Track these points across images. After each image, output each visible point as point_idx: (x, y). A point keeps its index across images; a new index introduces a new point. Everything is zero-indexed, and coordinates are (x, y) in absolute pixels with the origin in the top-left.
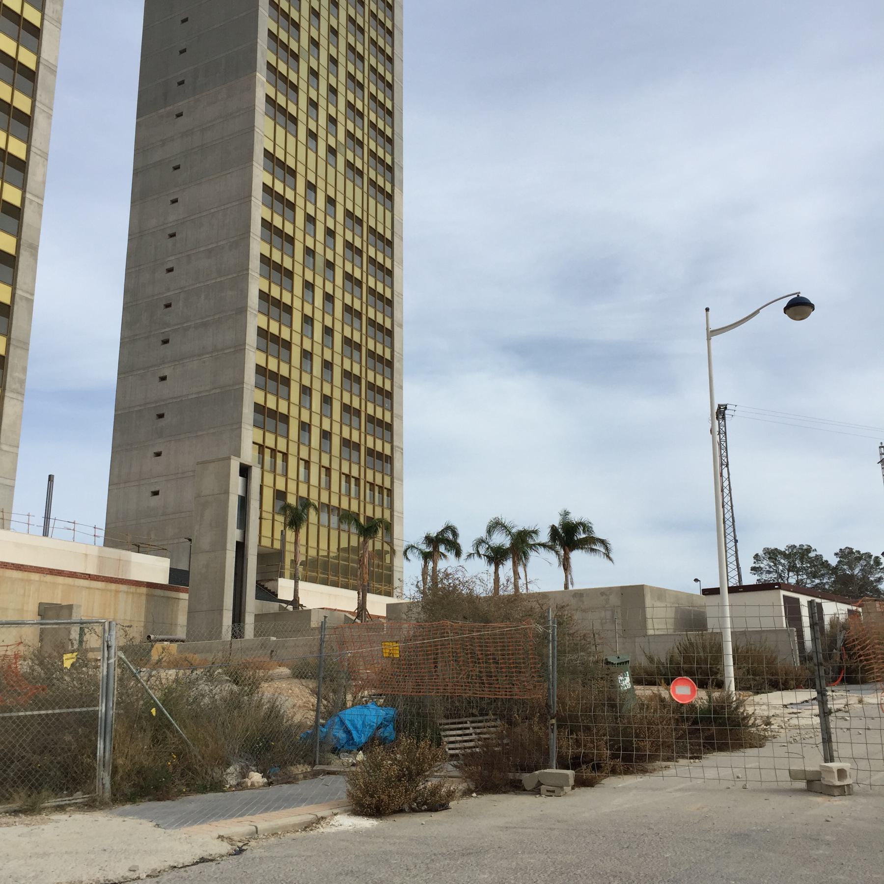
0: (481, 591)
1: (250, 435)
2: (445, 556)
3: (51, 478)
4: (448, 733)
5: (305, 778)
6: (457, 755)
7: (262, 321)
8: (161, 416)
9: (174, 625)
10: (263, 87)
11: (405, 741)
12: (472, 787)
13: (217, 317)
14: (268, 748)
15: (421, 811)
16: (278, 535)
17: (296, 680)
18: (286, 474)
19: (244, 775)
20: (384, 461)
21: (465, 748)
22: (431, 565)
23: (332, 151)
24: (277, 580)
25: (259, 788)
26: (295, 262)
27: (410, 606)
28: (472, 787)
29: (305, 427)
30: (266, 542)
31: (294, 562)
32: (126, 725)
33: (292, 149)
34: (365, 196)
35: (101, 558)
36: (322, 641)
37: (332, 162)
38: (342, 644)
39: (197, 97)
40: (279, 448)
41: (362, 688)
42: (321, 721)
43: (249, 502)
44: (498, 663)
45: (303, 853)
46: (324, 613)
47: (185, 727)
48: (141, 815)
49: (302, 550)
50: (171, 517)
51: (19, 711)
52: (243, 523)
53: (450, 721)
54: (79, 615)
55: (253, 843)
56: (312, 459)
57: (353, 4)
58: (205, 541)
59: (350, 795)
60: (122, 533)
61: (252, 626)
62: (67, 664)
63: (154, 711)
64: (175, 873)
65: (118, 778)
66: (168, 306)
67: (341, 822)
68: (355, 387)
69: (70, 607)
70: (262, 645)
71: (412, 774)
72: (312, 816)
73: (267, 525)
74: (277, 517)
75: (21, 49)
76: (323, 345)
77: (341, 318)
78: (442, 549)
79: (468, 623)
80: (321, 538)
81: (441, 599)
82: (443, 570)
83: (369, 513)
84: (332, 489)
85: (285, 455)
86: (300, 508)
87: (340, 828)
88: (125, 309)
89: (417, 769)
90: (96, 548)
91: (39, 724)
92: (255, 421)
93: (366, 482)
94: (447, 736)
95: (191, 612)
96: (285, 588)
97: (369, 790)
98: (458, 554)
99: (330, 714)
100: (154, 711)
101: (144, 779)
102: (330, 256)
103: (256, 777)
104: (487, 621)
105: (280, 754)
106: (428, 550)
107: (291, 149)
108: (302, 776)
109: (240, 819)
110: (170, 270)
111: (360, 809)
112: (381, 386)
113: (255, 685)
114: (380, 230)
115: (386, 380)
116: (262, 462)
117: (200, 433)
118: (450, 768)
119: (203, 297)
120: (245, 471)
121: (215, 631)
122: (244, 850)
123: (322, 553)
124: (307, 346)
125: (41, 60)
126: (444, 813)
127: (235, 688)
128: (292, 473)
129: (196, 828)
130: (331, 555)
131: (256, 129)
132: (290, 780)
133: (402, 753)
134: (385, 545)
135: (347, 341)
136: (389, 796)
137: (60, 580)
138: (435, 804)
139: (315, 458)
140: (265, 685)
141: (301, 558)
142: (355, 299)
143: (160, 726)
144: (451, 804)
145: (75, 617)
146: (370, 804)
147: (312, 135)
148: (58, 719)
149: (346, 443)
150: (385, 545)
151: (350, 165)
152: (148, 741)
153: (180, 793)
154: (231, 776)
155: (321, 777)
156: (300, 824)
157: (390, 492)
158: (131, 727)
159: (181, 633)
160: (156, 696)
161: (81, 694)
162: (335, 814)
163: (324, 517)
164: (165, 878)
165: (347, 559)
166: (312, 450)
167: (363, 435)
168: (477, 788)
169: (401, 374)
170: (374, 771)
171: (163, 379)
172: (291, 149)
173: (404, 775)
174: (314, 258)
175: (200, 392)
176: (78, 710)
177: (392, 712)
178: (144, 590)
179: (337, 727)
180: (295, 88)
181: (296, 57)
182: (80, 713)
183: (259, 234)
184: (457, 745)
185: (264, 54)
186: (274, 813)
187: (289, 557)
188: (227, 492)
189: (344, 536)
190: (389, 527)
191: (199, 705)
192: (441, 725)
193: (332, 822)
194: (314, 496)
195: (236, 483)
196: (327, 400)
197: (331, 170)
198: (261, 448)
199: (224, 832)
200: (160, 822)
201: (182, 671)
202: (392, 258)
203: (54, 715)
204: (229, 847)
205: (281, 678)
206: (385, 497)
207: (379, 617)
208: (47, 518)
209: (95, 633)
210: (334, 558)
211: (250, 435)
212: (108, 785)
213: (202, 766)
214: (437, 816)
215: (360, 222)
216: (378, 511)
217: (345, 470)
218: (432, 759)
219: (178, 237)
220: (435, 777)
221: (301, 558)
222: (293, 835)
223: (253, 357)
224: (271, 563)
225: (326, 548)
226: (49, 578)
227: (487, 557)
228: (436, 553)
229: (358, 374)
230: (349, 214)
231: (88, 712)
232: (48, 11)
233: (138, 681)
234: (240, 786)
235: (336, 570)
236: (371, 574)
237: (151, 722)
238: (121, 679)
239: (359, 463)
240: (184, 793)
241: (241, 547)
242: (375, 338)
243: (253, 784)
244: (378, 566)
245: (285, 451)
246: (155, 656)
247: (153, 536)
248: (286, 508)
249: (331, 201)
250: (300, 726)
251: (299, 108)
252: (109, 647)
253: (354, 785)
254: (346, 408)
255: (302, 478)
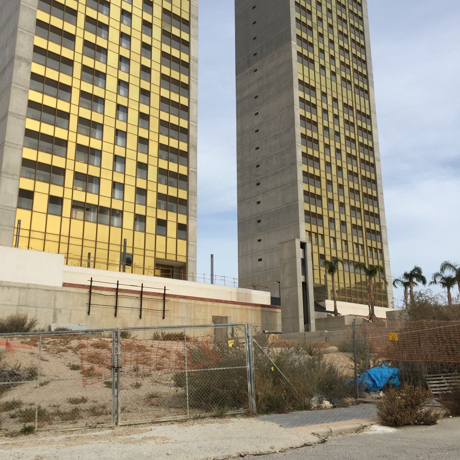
0: (442, 302)
1: (304, 227)
2: (416, 284)
3: (212, 256)
4: (431, 382)
5: (353, 404)
6: (437, 394)
7: (305, 168)
8: (259, 221)
9: (275, 325)
10: (295, 47)
11: (407, 386)
12: (449, 412)
13: (282, 168)
14: (331, 388)
15: (420, 425)
16: (323, 278)
17: (341, 353)
18: (324, 245)
19: (321, 402)
20: (376, 234)
21: (442, 390)
22: (409, 289)
23: (333, 74)
24: (325, 301)
25: (329, 409)
26: (319, 135)
27: (401, 312)
28: (449, 412)
29: (332, 220)
30: (317, 282)
31: (333, 291)
32: (260, 375)
33: (313, 76)
34: (353, 94)
35: (238, 293)
36: (354, 332)
37: (312, 67)
38: (365, 333)
39: (264, 59)
40: (319, 232)
41: (378, 357)
42: (358, 375)
43: (307, 261)
44: (457, 343)
45: (357, 444)
46: (354, 317)
47: (288, 377)
48: (272, 420)
49: (336, 284)
50: (269, 271)
51: (211, 368)
52: (305, 272)
53: (431, 375)
54: (231, 321)
55: (330, 437)
56: (337, 236)
57: (351, 3)
58: (287, 283)
59: (379, 414)
60: (247, 280)
61: (314, 325)
62: (230, 345)
63: (272, 368)
64: (292, 451)
65: (259, 401)
66: (258, 166)
67: (376, 429)
68: (357, 196)
69: (226, 318)
70: (321, 335)
71: (414, 404)
72: (359, 425)
73: (317, 272)
74: (321, 268)
75: (182, 54)
76: (337, 176)
77: (345, 161)
78: (415, 280)
79: (436, 321)
80: (346, 278)
81: (419, 309)
82: (418, 292)
83: (371, 263)
84: (326, 246)
85: (323, 236)
86: (333, 262)
87: (375, 432)
88: (238, 170)
89: (416, 401)
90: (235, 288)
91: (220, 374)
92: (305, 219)
93: (367, 246)
94: (429, 384)
95: (283, 319)
96: (329, 305)
97: (389, 412)
98: (424, 282)
99: (362, 371)
100: (272, 368)
101: (272, 402)
102: (337, 129)
103: (327, 403)
104: (448, 320)
105: (340, 392)
106: (406, 281)
107: (312, 77)
108: (351, 403)
109: (322, 425)
110: (257, 148)
111: (386, 422)
112: (371, 194)
113: (320, 356)
114: (363, 110)
115: (373, 191)
116: (311, 240)
117: (279, 228)
118: (435, 401)
119: (274, 159)
120: (303, 245)
121: (296, 329)
122: (326, 441)
123: (347, 286)
124: (329, 178)
125: (191, 57)
126: (434, 426)
127: (310, 357)
128: (327, 245)
129: (300, 428)
130: (352, 286)
131: (294, 70)
132: (345, 405)
133: (406, 393)
134: (381, 280)
135: (350, 173)
136: (401, 416)
137: (221, 304)
138: (428, 421)
139: (338, 236)
140: (325, 355)
141: (336, 289)
142: (352, 150)
143: (276, 377)
144: (438, 421)
145: (229, 323)
146: (391, 419)
147: (323, 67)
148: (228, 372)
149: (354, 226)
150: (381, 280)
151: (344, 79)
152: (271, 384)
153: (289, 410)
154: (314, 402)
155: (361, 404)
156: (353, 429)
157: (381, 251)
158: (263, 377)
159: (279, 329)
160: (272, 360)
161: (238, 360)
162: (372, 425)
163: (346, 266)
164: (288, 453)
165: (361, 288)
166: (336, 232)
167: (363, 222)
168: (452, 413)
169: (381, 186)
170: (391, 402)
171: (259, 203)
172: (312, 77)
173: (409, 405)
174: (329, 131)
175: (277, 207)
176: (237, 367)
177: (396, 370)
178: (259, 308)
179: (367, 378)
180: (312, 45)
181: (311, 28)
182: (238, 369)
183: (299, 123)
184: (437, 389)
185: (295, 30)
186: (338, 422)
187: (329, 289)
188: (295, 257)
189: (358, 276)
190: (382, 270)
191: (294, 366)
192: (426, 377)
193: (371, 429)
194: (340, 256)
195: (299, 252)
196: (342, 205)
197: (334, 84)
198: (310, 233)
199: (315, 431)
200: (282, 424)
201: (284, 348)
202: (371, 124)
203: (227, 370)
204: (318, 439)
205: (333, 352)
206: (379, 254)
207: (382, 319)
208: (212, 275)
209: (241, 330)
210: (354, 288)
211: (304, 227)
212: (255, 405)
213: (298, 397)
214: (430, 428)
215: (352, 108)
216: (376, 261)
217: (355, 241)
218: (424, 397)
219: (260, 131)
220: (427, 406)
221: (336, 289)
222: (350, 435)
223: (302, 187)
224: (321, 292)
225: (349, 283)
226: (216, 304)
227: (442, 283)
228: (411, 283)
229: (359, 207)
230: (345, 105)
231: (242, 369)
232: (192, 33)
233: (263, 353)
234: (319, 408)
235: (355, 294)
236: (375, 295)
237: (273, 374)
238: (255, 353)
239: (363, 237)
240: (291, 410)
241: (305, 285)
242: (365, 169)
243: (325, 407)
244: (379, 291)
245: (322, 234)
246: (270, 341)
247: (261, 281)
248: (326, 262)
249: (335, 100)
250: (347, 377)
251: (314, 55)
252: (248, 337)
253: (381, 409)
254: (353, 208)
255: (332, 246)
